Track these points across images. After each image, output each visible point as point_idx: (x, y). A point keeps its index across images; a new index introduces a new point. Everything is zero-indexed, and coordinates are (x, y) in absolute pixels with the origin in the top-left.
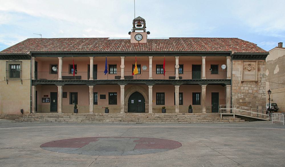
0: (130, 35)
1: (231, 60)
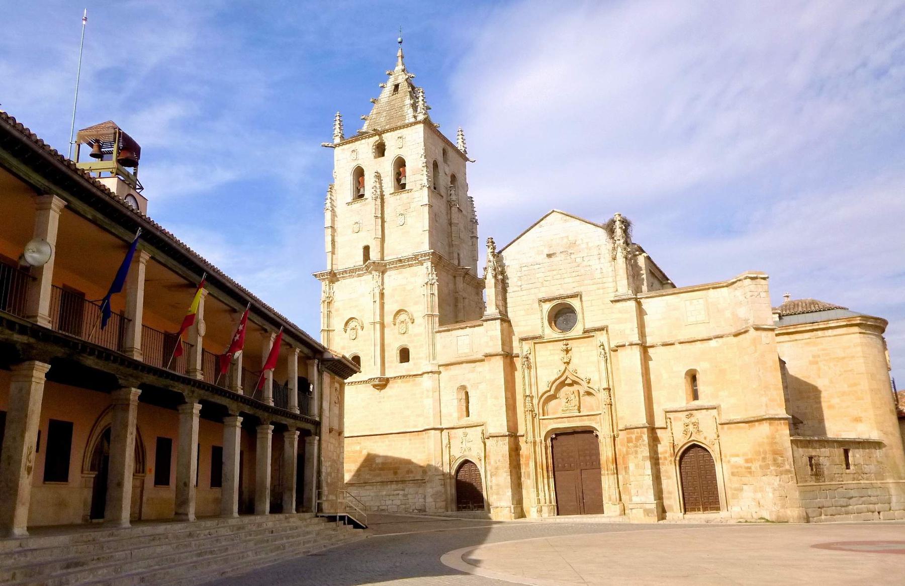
0: (469, 194)
1: (320, 373)
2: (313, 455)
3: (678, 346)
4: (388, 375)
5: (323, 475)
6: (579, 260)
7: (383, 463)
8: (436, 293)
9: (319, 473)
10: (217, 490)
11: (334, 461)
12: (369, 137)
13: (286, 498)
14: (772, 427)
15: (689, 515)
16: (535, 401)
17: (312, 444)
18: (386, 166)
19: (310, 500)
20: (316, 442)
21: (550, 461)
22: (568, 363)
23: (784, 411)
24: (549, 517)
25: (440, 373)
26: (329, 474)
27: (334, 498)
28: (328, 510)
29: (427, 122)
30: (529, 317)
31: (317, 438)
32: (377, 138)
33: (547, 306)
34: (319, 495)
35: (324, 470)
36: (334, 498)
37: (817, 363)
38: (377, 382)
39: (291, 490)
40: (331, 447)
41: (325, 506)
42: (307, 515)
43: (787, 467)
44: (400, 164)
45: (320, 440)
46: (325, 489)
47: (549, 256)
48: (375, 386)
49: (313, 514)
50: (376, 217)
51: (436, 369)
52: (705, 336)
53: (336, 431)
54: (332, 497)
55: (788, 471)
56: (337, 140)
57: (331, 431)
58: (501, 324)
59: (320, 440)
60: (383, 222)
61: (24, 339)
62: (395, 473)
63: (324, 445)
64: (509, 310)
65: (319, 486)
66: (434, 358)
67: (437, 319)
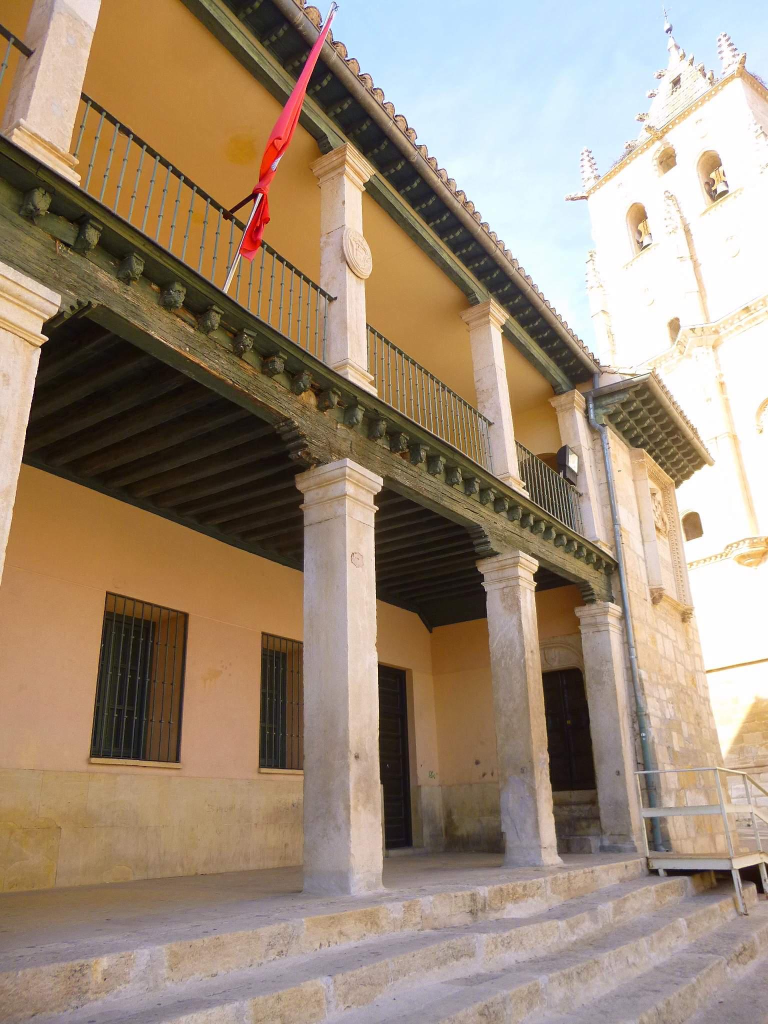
1: (595, 430)
2: (610, 661)
5: (654, 724)
9: (638, 717)
10: (286, 785)
11: (681, 690)
12: (643, 150)
13: (510, 800)
17: (600, 628)
18: (687, 177)
19: (621, 808)
20: (613, 621)
26: (671, 725)
27: (702, 800)
28: (690, 844)
29: (743, 73)
31: (614, 609)
32: (658, 144)
34: (650, 791)
35: (652, 707)
36: (702, 800)
38: (745, 549)
39: (526, 770)
40: (665, 647)
41: (677, 828)
42: (607, 873)
45: (624, 617)
46: (669, 776)
48: (742, 558)
49: (633, 865)
53: (675, 606)
54: (694, 798)
57: (657, 597)
59: (624, 617)
60: (696, 265)
63: (640, 634)
65: (644, 759)
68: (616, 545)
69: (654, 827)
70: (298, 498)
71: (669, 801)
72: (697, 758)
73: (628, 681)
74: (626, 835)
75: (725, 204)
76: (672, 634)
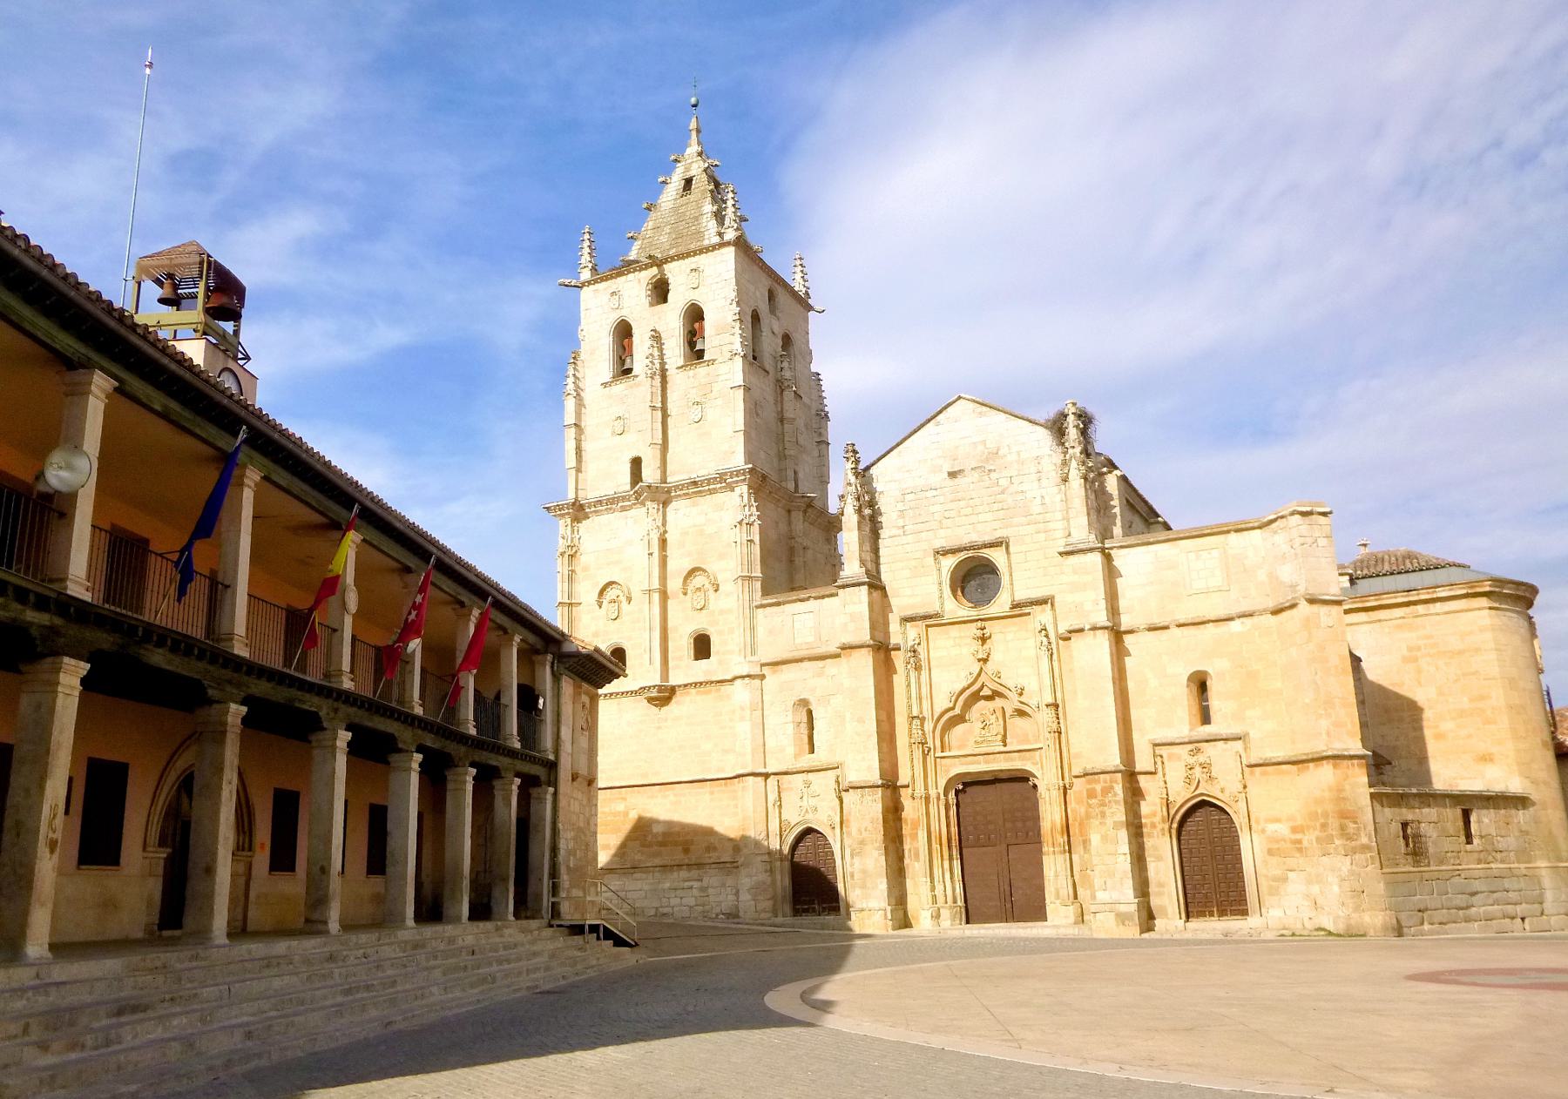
0: (813, 369)
1: (556, 677)
3: (1175, 631)
4: (673, 681)
5: (562, 853)
6: (1004, 482)
7: (664, 834)
8: (757, 539)
9: (554, 850)
11: (580, 830)
13: (496, 893)
14: (1338, 772)
15: (1195, 924)
16: (929, 726)
17: (542, 800)
19: (539, 896)
20: (549, 798)
21: (954, 830)
22: (985, 661)
23: (1359, 745)
24: (952, 927)
25: (763, 677)
26: (571, 853)
27: (581, 894)
28: (569, 914)
29: (741, 244)
30: (917, 582)
31: (551, 790)
32: (654, 270)
33: (950, 562)
34: (555, 889)
35: (562, 845)
36: (581, 894)
37: (1416, 660)
38: (654, 694)
39: (505, 880)
41: (565, 908)
43: (1364, 840)
44: (695, 315)
45: (555, 794)
46: (565, 879)
47: (952, 475)
48: (650, 700)
50: (653, 408)
51: (756, 670)
52: (1222, 613)
54: (576, 893)
55: (1365, 848)
56: (586, 275)
57: (574, 777)
58: (870, 593)
59: (555, 794)
61: (43, 618)
62: (686, 851)
63: (562, 803)
64: (883, 568)
65: (554, 874)
66: (753, 653)
67: (758, 585)
68: (557, 752)
69: (555, 906)
70: (493, 788)
71: (563, 894)
72: (585, 869)
73: (1014, 774)
74: (539, 911)
75: (701, 370)
76: (580, 796)
